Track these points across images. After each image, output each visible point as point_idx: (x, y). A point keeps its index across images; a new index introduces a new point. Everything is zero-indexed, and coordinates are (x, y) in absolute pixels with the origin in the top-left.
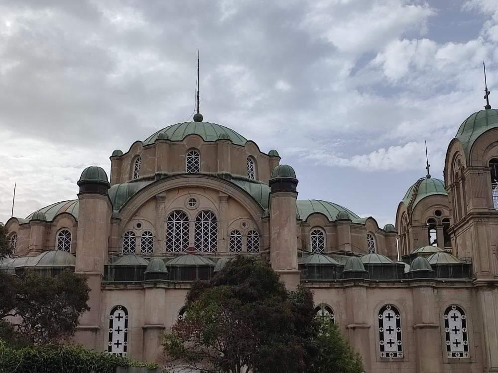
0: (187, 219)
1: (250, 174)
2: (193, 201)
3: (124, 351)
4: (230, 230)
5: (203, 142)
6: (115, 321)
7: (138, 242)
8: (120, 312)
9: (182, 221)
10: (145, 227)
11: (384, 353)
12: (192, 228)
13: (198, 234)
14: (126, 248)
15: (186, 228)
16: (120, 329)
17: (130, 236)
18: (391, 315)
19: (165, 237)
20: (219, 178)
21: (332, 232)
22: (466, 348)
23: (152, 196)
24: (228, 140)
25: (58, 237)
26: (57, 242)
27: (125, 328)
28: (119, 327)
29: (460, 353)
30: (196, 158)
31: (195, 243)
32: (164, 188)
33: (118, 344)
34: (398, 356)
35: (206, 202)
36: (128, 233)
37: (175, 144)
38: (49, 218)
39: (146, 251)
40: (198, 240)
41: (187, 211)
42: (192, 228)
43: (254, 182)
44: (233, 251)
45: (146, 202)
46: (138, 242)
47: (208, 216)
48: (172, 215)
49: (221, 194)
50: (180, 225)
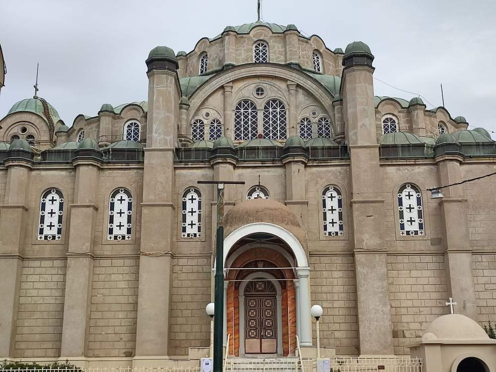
0: (255, 108)
1: (316, 63)
2: (260, 91)
3: (58, 234)
4: (300, 118)
5: (271, 34)
6: (328, 201)
7: (207, 130)
8: (409, 189)
9: (250, 111)
10: (214, 115)
11: (43, 237)
12: (260, 116)
13: (282, 122)
14: (195, 136)
15: (254, 117)
16: (194, 211)
17: (198, 125)
18: (120, 198)
19: (233, 126)
20: (288, 66)
21: (408, 117)
22: (129, 231)
23: (220, 85)
24: (295, 30)
25: (126, 129)
26: (125, 133)
27: (199, 209)
28: (192, 209)
29: (122, 236)
30: (264, 49)
31: (264, 132)
32: (228, 80)
33: (192, 224)
34: (419, 234)
35: (273, 90)
36: (197, 121)
37: (242, 37)
38: (117, 111)
39: (214, 139)
40: (266, 128)
41: (254, 99)
42: (260, 116)
43: (317, 73)
44: (246, 139)
45: (217, 89)
46: (207, 130)
47: (277, 105)
48: (240, 104)
49: (289, 83)
50: (277, 113)
